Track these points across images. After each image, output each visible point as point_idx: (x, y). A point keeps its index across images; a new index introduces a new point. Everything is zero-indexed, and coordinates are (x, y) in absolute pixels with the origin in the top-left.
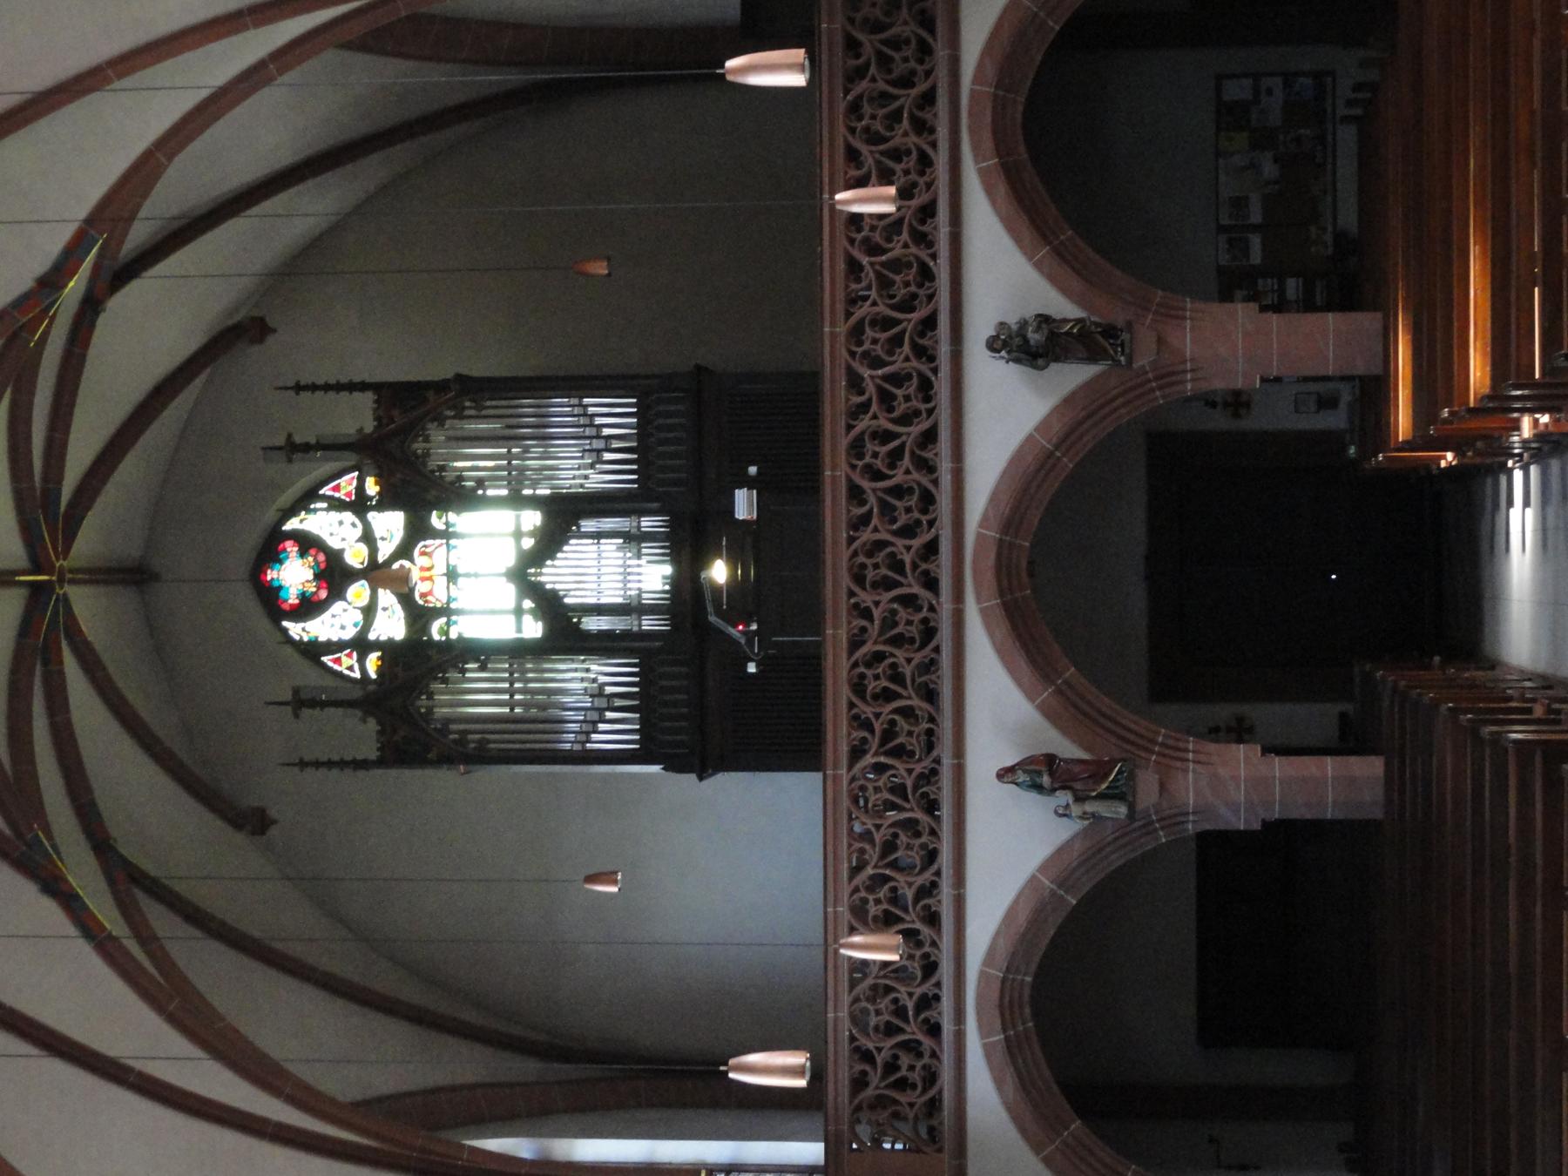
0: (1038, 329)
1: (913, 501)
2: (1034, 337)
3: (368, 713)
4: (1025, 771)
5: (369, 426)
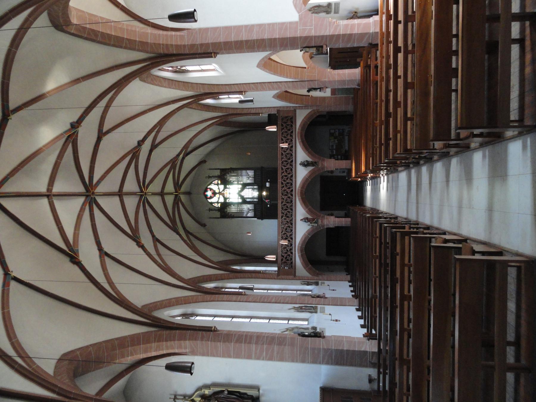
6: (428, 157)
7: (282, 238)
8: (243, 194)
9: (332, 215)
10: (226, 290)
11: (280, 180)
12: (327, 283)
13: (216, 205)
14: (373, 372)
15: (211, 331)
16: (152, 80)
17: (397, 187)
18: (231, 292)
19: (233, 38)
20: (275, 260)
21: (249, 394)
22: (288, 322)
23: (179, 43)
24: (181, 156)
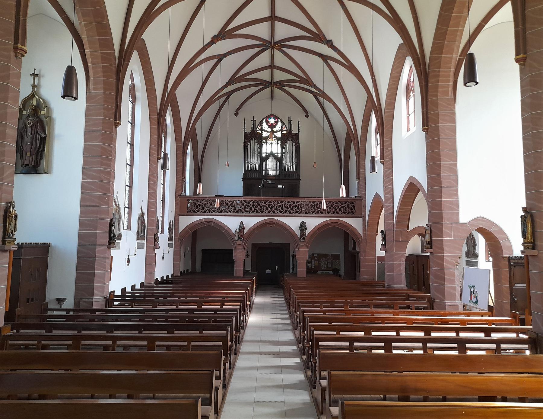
6: (310, 364)
7: (222, 201)
8: (271, 158)
9: (247, 256)
10: (163, 138)
11: (285, 199)
12: (172, 250)
13: (259, 128)
14: (69, 303)
15: (116, 119)
16: (400, 58)
17: (277, 330)
18: (161, 143)
19: (443, 150)
20: (198, 193)
21: (42, 161)
22: (127, 207)
23: (440, 90)
24: (314, 90)
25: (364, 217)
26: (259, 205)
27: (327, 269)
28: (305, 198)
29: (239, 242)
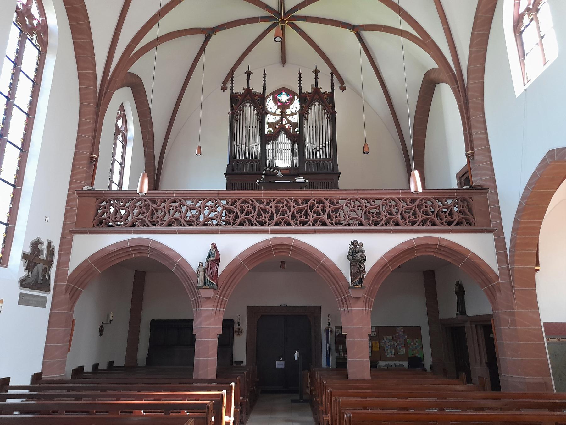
0: (362, 257)
1: (303, 218)
2: (358, 255)
3: (246, 90)
4: (215, 252)
5: (322, 91)
8: (282, 138)
25: (497, 231)
26: (254, 209)
27: (398, 357)
28: (358, 192)
29: (207, 293)
